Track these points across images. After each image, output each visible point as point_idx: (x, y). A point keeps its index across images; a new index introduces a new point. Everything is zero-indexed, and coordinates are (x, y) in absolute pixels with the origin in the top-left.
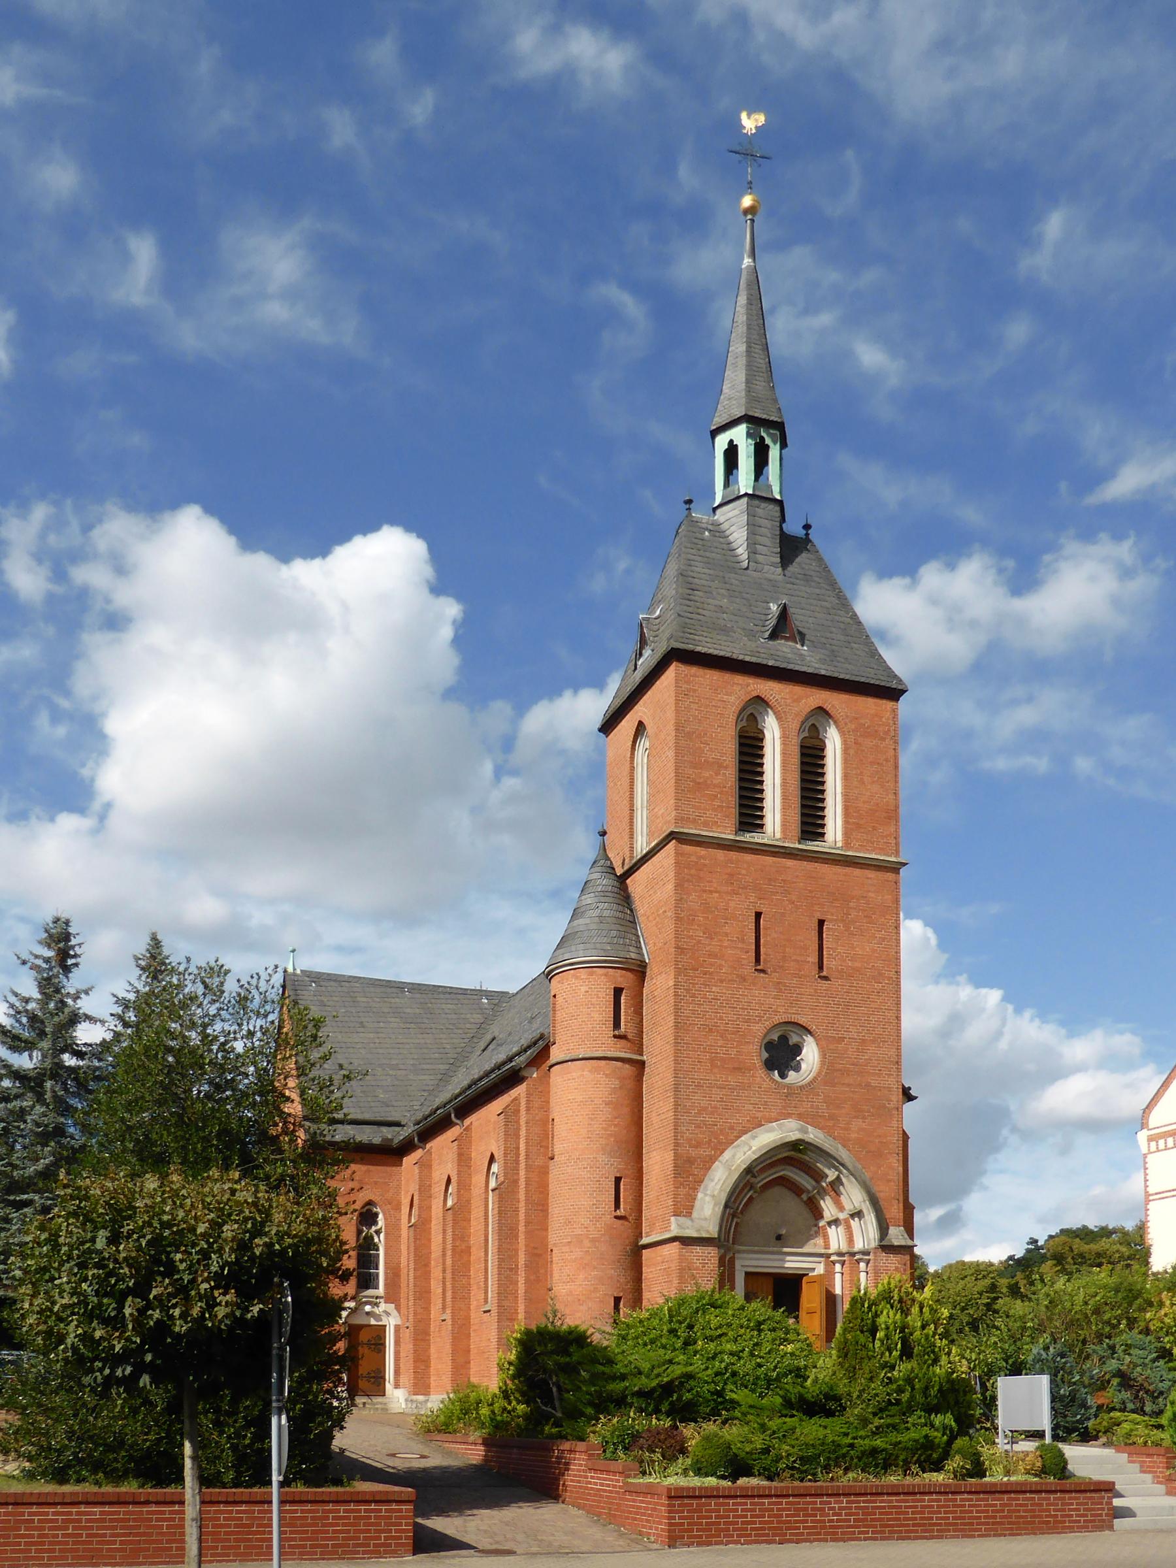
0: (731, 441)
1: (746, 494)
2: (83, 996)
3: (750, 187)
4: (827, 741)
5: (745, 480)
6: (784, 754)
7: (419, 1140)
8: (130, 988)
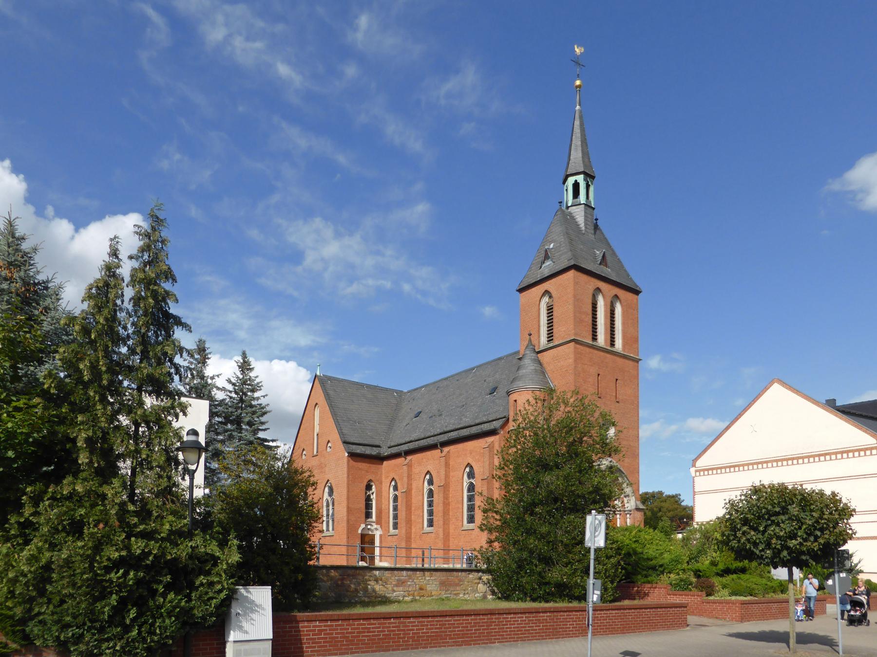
0: (576, 181)
1: (584, 204)
2: (216, 378)
5: (582, 198)
6: (605, 311)
8: (234, 376)
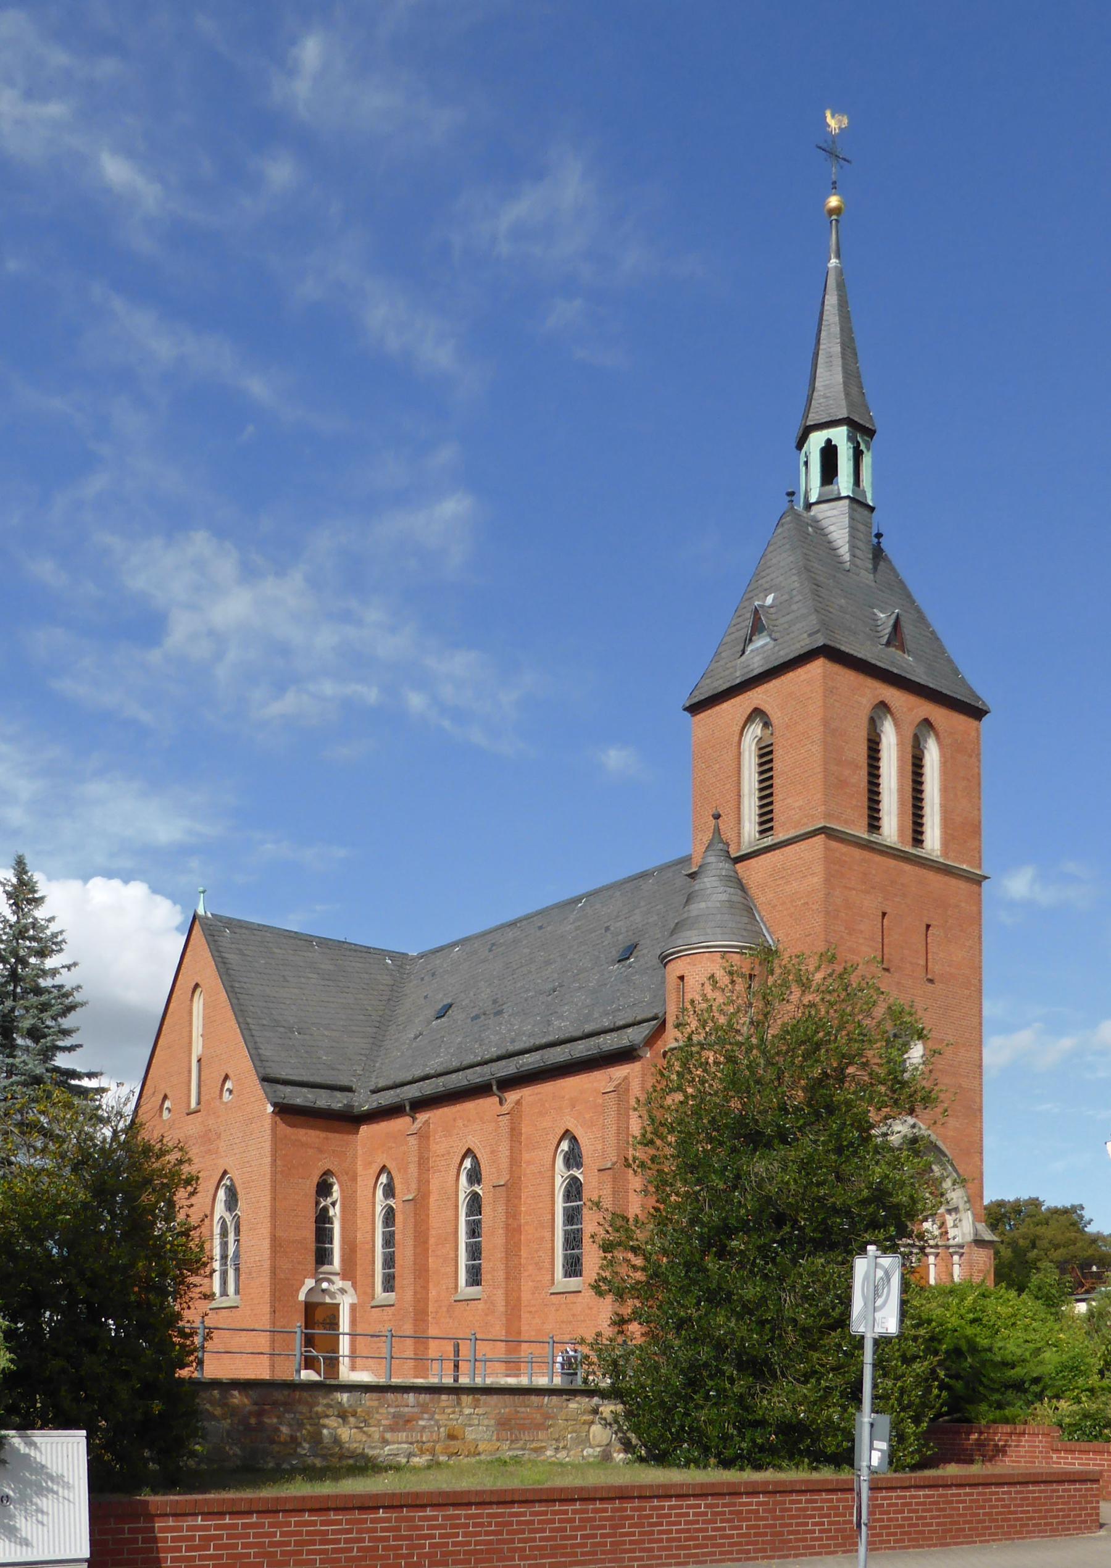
0: (829, 441)
1: (848, 497)
3: (834, 187)
4: (926, 752)
7: (411, 1109)
